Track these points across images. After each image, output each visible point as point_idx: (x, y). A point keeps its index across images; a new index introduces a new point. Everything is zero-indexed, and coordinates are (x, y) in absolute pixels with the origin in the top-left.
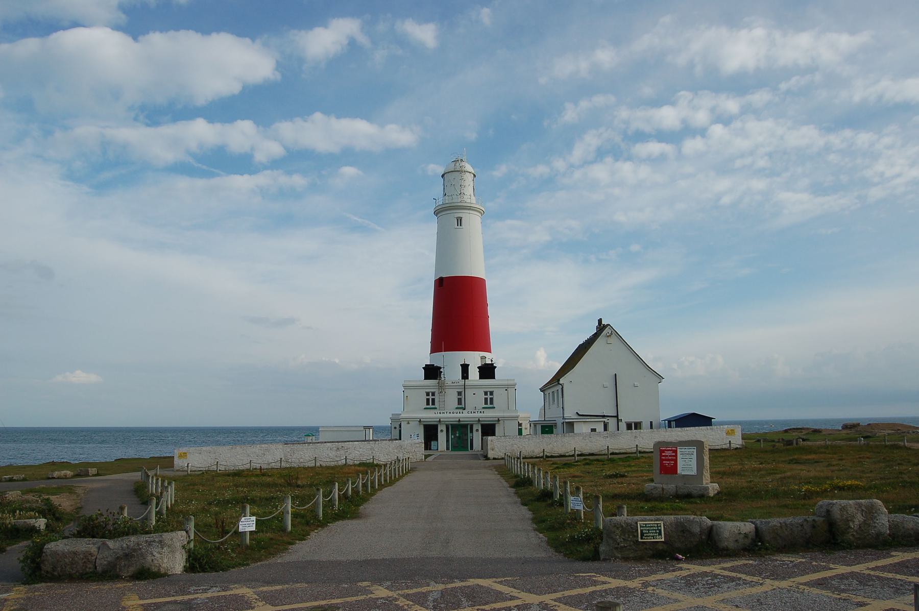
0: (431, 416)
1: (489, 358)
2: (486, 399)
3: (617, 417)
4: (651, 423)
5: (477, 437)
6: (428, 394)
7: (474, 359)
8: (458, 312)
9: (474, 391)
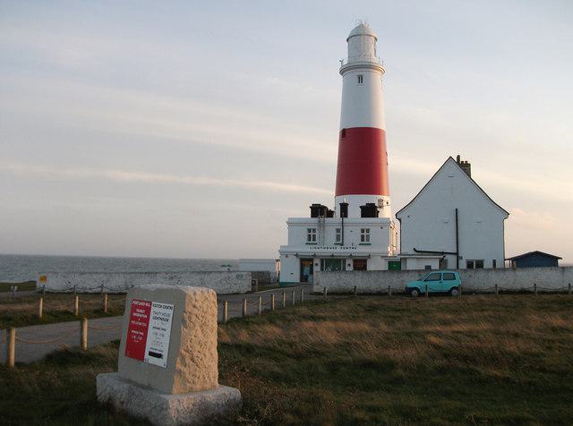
0: (308, 250)
2: (363, 236)
3: (457, 254)
6: (309, 230)
8: (360, 156)
9: (351, 228)
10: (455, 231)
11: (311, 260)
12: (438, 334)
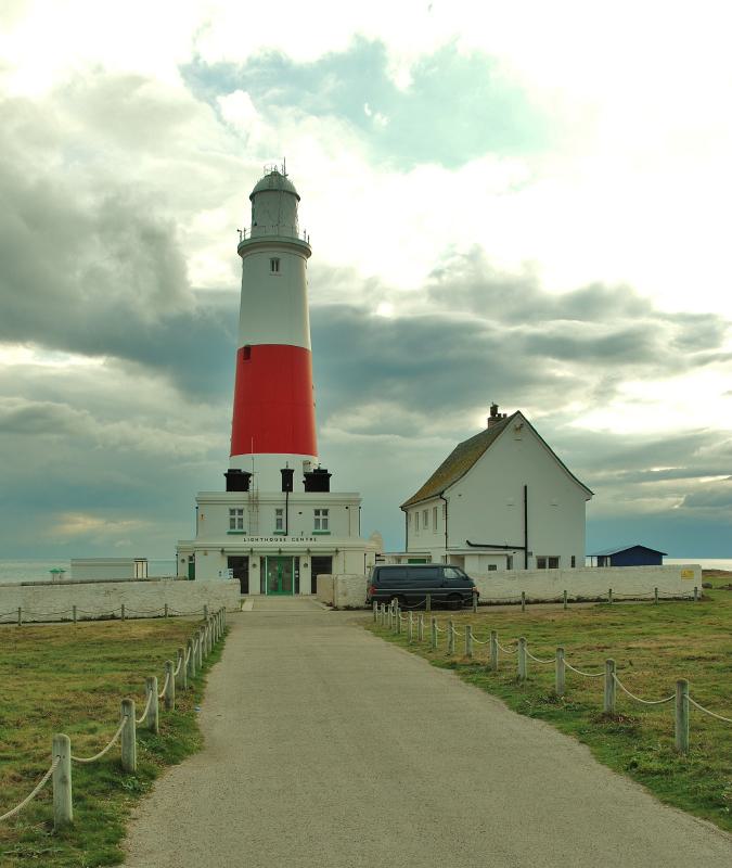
0: (238, 545)
1: (316, 462)
2: (317, 521)
3: (525, 548)
4: (573, 558)
5: (305, 575)
6: (232, 512)
7: (295, 461)
9: (300, 509)
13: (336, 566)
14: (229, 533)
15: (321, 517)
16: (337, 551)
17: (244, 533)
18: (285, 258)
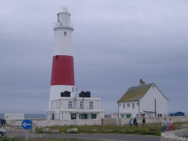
0: (73, 110)
2: (90, 105)
3: (155, 112)
6: (69, 102)
9: (87, 102)
10: (155, 102)
11: (76, 114)
12: (63, 134)
13: (97, 116)
14: (69, 108)
15: (91, 104)
16: (98, 113)
17: (72, 108)
18: (68, 32)
